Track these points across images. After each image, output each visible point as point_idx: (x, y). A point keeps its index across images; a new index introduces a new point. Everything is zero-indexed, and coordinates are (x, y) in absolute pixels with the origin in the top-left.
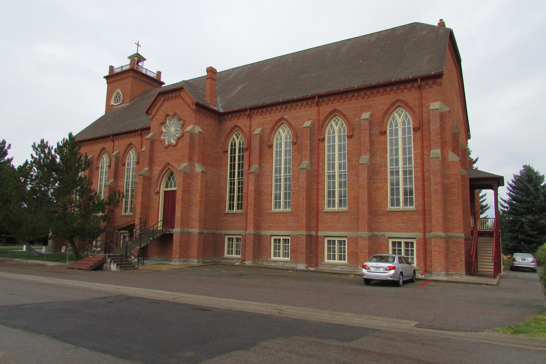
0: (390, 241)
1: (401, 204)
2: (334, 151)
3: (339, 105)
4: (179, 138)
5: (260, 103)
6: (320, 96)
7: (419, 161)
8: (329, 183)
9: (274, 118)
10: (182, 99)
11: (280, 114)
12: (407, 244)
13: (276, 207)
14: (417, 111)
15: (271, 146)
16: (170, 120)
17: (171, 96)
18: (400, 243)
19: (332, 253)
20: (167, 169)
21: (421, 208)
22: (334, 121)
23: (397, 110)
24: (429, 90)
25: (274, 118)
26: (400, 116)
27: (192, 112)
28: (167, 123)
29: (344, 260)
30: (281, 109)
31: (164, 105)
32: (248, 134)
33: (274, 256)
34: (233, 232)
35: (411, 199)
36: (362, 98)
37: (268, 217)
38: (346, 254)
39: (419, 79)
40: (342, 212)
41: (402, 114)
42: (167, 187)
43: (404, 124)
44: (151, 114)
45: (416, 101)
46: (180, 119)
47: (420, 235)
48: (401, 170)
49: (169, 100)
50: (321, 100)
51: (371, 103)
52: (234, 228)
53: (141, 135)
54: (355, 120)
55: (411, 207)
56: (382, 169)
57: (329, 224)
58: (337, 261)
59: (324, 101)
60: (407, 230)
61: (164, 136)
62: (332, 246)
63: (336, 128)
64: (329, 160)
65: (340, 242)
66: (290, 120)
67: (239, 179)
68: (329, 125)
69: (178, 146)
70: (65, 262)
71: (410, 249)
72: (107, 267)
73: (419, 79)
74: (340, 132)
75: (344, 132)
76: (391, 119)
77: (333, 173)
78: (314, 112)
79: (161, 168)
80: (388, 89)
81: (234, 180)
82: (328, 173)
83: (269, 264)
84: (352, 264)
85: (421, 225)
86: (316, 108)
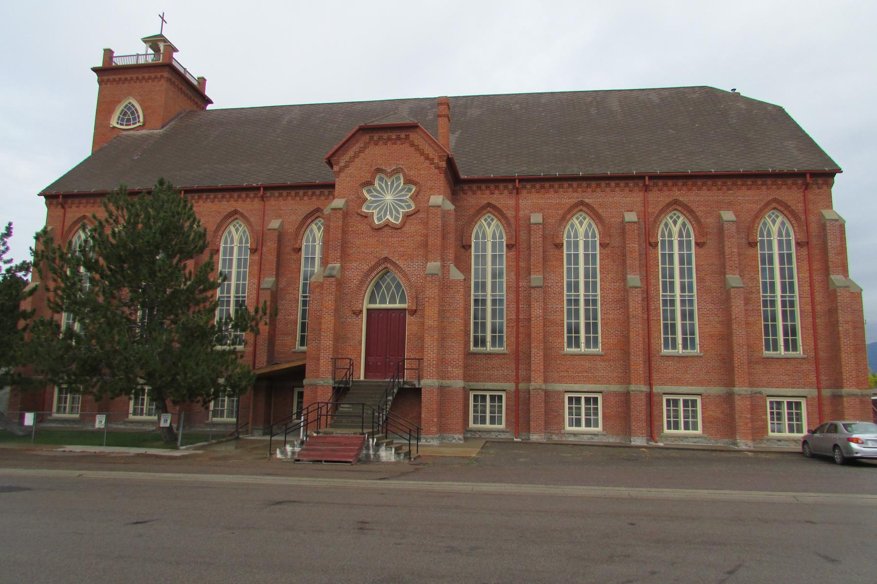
0: (567, 396)
2: (576, 263)
3: (679, 194)
4: (407, 216)
6: (653, 177)
7: (807, 288)
8: (476, 311)
9: (564, 201)
10: (412, 145)
11: (575, 195)
12: (588, 400)
13: (569, 345)
14: (803, 217)
15: (559, 246)
16: (381, 179)
17: (385, 136)
18: (578, 400)
20: (380, 268)
21: (812, 354)
22: (234, 226)
24: (817, 191)
25: (564, 201)
27: (437, 171)
28: (376, 185)
30: (215, 198)
32: (512, 221)
33: (474, 423)
34: (489, 385)
36: (719, 190)
37: (558, 362)
40: (687, 357)
42: (372, 300)
44: (337, 164)
45: (799, 204)
47: (511, 386)
48: (678, 300)
49: (381, 143)
50: (268, 194)
51: (732, 198)
52: (490, 379)
54: (708, 220)
56: (754, 296)
57: (670, 376)
60: (793, 385)
61: (368, 208)
62: (592, 406)
63: (236, 237)
67: (237, 297)
68: (227, 231)
69: (405, 229)
70: (176, 448)
71: (497, 404)
72: (368, 455)
74: (241, 242)
75: (247, 242)
76: (308, 232)
78: (639, 199)
79: (366, 268)
80: (759, 182)
81: (230, 297)
82: (304, 297)
83: (564, 439)
84: (712, 435)
85: (813, 378)
86: (641, 194)
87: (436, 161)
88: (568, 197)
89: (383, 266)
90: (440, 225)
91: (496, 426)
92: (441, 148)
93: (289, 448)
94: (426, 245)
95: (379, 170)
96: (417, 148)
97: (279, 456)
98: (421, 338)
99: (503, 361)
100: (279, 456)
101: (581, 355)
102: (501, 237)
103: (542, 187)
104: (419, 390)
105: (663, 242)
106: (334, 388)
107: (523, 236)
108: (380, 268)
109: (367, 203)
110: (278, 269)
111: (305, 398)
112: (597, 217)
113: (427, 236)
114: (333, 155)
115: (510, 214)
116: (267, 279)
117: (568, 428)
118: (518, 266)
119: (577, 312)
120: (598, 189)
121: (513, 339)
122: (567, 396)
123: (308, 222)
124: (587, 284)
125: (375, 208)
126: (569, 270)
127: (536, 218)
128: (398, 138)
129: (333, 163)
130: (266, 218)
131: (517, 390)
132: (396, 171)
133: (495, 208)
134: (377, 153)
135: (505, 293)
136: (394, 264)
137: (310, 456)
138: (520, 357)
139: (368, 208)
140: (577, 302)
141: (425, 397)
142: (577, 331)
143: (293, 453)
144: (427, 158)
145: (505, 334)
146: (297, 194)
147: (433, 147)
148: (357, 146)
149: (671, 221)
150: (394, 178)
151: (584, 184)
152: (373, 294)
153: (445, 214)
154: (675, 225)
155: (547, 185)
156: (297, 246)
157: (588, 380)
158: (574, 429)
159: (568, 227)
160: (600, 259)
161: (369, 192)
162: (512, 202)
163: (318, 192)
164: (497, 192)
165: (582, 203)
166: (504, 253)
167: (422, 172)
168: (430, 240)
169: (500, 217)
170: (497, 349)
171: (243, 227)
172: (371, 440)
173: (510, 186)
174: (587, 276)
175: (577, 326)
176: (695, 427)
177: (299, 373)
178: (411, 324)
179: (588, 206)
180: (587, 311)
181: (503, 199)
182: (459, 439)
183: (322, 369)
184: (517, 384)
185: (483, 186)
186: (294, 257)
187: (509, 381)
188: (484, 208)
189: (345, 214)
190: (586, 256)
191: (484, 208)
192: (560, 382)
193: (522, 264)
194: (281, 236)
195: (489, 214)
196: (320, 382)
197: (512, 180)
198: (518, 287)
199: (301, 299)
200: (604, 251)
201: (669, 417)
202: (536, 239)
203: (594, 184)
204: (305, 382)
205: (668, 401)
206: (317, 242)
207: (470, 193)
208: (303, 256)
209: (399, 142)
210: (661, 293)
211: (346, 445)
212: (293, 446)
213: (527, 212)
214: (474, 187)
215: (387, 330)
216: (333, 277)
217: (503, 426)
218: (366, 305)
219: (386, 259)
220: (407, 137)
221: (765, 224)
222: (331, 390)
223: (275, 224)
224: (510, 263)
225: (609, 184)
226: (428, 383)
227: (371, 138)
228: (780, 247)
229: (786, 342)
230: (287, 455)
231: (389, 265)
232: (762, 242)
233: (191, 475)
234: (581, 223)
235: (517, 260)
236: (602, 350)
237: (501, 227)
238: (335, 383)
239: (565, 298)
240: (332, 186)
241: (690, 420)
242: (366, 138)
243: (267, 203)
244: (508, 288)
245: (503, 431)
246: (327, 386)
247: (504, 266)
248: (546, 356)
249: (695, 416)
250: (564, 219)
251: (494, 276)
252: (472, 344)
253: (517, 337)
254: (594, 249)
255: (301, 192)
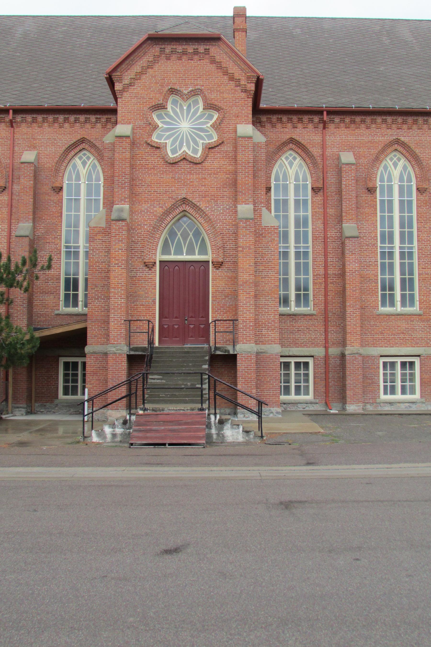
1: (80, 303)
4: (210, 148)
5: (352, 103)
10: (213, 61)
12: (298, 365)
13: (384, 304)
15: (371, 191)
17: (180, 48)
18: (393, 365)
19: (70, 384)
20: (177, 211)
23: (81, 154)
25: (376, 139)
26: (84, 164)
27: (243, 95)
28: (169, 109)
29: (307, 393)
31: (156, 67)
32: (319, 160)
35: (412, 297)
37: (372, 323)
38: (382, 384)
39: (11, 112)
41: (89, 163)
42: (166, 250)
43: (89, 178)
44: (120, 81)
46: (210, 106)
47: (320, 352)
50: (19, 118)
53: (12, 124)
55: (306, 309)
58: (399, 396)
59: (24, 121)
63: (83, 172)
64: (68, 226)
65: (298, 365)
66: (412, 146)
67: (67, 247)
69: (206, 164)
72: (209, 436)
73: (11, 112)
76: (70, 167)
77: (75, 247)
79: (159, 211)
82: (67, 247)
83: (379, 408)
87: (243, 82)
88: (380, 133)
89: (181, 209)
90: (251, 161)
91: (302, 397)
92: (249, 67)
93: (108, 430)
94: (235, 183)
95: (172, 91)
96: (219, 66)
97: (95, 438)
98: (234, 295)
99: (311, 322)
100: (95, 438)
101: (398, 315)
102: (305, 180)
103: (353, 122)
104: (234, 357)
105: (382, 187)
106: (127, 355)
107: (331, 179)
108: (177, 211)
109: (157, 132)
110: (34, 213)
111: (88, 368)
112: (413, 158)
113: (235, 172)
114: (115, 69)
115: (316, 151)
116: (21, 224)
117: (383, 397)
118: (325, 213)
119: (391, 266)
120: (415, 127)
121: (322, 298)
122: (382, 360)
123: (70, 156)
124: (402, 234)
125: (168, 138)
126: (382, 218)
127: (347, 157)
128: (196, 52)
129: (115, 79)
130: (16, 149)
131: (327, 357)
132: (194, 93)
133: (298, 144)
134: (170, 68)
135: (310, 244)
136: (195, 206)
137: (147, 438)
138: (334, 317)
139: (210, 137)
140: (391, 254)
141: (241, 365)
142: (392, 288)
143: (114, 435)
144: (232, 78)
145: (311, 293)
146: (55, 120)
147: (238, 66)
148: (145, 59)
149: (391, 163)
150: (190, 101)
151: (400, 119)
152: (166, 242)
153: (256, 146)
154: (84, 166)
155: (358, 119)
156: (58, 185)
157: (404, 343)
158: (389, 397)
159: (381, 168)
160: (418, 207)
161: (160, 117)
162: (317, 138)
163: (82, 118)
164: (299, 125)
165: (397, 141)
166: (309, 197)
167: (225, 95)
168: (239, 178)
169: (304, 156)
170: (302, 309)
171: (92, 160)
172: (212, 417)
173: (316, 119)
174: (402, 226)
175: (392, 282)
176: (413, 392)
177: (76, 340)
178: (216, 281)
179: (403, 145)
180: (402, 265)
181: (307, 133)
182: (277, 413)
183: (113, 333)
184: (326, 348)
185: (285, 118)
186: (54, 197)
187: (317, 345)
188: (285, 144)
189: (133, 142)
190: (401, 203)
191: (285, 144)
192: (374, 345)
193: (331, 211)
194: (37, 171)
195: (291, 152)
196: (109, 351)
197: (319, 112)
198: (325, 238)
199: (63, 250)
200: (422, 198)
201: (385, 381)
202: (348, 181)
203: (410, 120)
204: (87, 349)
205: (385, 364)
206: (82, 180)
207: (268, 126)
208: (65, 197)
209: (196, 57)
210: (379, 244)
211: (186, 424)
212: (113, 425)
213: (335, 150)
214: (274, 118)
215: (185, 288)
216: (123, 220)
217: (310, 397)
218: (159, 257)
219: (185, 201)
220: (207, 51)
221: (386, 168)
222: (125, 359)
223: (29, 156)
224: (317, 210)
225: (427, 121)
226: (244, 349)
227: (162, 51)
228: (401, 193)
229: (403, 297)
230: (105, 438)
231: (188, 208)
232: (382, 187)
233: (65, 469)
234: (395, 165)
235: (325, 206)
236: (420, 308)
237: (305, 168)
238: (131, 349)
239: (379, 250)
240: (114, 111)
241: (302, 384)
242: (155, 50)
243: (17, 130)
244: (315, 238)
245: (311, 403)
246: (120, 355)
247: (309, 214)
248: (362, 318)
249: (412, 380)
250: (377, 159)
251: (297, 225)
252: (62, 303)
253: (326, 295)
254: (410, 194)
255: (61, 118)
